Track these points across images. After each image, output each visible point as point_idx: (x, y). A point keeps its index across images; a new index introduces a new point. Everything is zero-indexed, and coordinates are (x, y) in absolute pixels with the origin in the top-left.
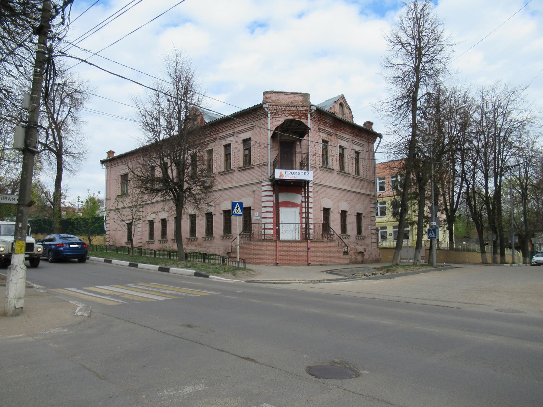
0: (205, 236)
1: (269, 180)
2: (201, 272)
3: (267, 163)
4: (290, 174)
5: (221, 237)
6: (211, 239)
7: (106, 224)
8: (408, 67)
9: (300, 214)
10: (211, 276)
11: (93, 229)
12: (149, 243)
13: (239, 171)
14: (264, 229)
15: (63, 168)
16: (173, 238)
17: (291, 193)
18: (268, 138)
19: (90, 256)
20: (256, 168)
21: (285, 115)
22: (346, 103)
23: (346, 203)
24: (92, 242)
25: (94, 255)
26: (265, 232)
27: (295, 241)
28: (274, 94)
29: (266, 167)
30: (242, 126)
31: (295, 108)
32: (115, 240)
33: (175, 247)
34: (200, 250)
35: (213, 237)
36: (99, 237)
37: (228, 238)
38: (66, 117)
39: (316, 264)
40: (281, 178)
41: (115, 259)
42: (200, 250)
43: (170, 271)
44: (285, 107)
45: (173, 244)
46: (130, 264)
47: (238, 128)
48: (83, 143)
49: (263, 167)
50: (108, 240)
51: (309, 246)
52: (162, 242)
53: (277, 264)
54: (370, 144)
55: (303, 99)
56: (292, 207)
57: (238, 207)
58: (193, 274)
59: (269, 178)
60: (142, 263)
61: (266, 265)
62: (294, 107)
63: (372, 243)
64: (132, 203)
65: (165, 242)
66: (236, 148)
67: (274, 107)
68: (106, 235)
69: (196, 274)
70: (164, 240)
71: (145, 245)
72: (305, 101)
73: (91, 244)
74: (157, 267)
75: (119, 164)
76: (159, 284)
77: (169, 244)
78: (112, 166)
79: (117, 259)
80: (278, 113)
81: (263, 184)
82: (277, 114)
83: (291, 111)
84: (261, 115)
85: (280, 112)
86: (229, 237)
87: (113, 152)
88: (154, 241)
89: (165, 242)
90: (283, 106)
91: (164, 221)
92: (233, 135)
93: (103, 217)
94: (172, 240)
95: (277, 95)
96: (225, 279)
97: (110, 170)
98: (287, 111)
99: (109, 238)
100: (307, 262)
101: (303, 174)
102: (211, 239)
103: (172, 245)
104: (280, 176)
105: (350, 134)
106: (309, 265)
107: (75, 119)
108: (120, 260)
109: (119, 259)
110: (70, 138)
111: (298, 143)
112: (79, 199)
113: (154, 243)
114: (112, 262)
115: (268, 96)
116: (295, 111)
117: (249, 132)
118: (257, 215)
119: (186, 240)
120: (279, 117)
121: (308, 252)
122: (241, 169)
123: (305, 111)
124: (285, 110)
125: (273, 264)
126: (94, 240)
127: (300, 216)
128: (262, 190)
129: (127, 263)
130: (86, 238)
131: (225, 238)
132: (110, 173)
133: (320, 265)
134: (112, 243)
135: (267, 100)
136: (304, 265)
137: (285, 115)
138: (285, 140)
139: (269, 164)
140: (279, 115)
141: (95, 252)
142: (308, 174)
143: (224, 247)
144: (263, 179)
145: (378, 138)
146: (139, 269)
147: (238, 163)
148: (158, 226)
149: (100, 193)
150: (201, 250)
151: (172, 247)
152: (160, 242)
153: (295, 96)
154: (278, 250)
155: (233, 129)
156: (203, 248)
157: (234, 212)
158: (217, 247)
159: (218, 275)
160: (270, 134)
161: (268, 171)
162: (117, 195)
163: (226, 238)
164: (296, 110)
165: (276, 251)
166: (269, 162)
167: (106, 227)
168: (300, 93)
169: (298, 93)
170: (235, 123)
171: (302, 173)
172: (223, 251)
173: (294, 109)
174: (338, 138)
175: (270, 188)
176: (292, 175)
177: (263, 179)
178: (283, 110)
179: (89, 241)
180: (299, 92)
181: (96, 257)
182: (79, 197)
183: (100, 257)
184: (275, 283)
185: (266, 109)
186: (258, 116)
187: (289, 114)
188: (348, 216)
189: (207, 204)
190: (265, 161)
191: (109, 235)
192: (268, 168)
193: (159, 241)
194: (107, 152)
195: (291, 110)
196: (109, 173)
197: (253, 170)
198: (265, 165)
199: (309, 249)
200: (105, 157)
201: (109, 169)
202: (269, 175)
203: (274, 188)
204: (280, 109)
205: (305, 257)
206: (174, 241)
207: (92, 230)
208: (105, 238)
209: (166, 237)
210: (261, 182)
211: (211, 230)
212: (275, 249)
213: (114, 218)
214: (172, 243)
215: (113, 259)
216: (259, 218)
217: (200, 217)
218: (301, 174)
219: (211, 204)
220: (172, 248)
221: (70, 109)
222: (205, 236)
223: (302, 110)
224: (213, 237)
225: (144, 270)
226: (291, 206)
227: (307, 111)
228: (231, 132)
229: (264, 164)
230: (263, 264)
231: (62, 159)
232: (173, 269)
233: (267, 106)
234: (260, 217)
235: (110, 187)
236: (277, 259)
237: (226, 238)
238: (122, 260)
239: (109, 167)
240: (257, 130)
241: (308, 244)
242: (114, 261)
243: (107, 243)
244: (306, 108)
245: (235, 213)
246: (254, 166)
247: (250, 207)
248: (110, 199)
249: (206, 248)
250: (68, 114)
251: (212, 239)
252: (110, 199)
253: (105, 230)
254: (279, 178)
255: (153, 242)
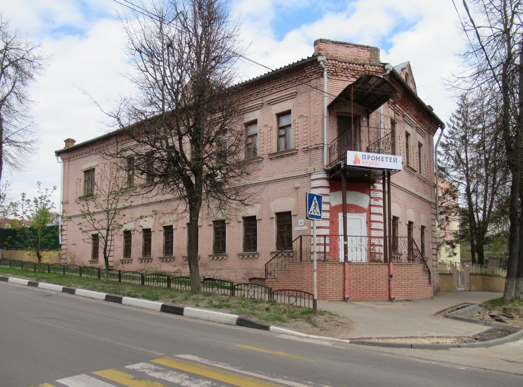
0: (212, 254)
1: (325, 170)
2: (249, 319)
3: (322, 145)
4: (370, 159)
5: (239, 255)
6: (223, 257)
7: (62, 236)
8: (495, 30)
9: (367, 223)
10: (272, 328)
11: (44, 241)
12: (124, 262)
13: (271, 159)
14: (325, 245)
15: (4, 161)
16: (162, 256)
17: (354, 192)
18: (323, 108)
19: (40, 281)
20: (300, 153)
21: (347, 77)
22: (412, 74)
23: (412, 211)
24: (42, 259)
25: (46, 280)
26: (323, 249)
27: (361, 264)
28: (330, 45)
29: (320, 151)
30: (278, 93)
31: (361, 67)
32: (75, 256)
33: (186, 271)
34: (204, 273)
35: (225, 255)
36: (51, 253)
37: (251, 257)
38: (9, 94)
39: (401, 299)
40: (357, 165)
41: (81, 288)
42: (204, 273)
43: (184, 313)
44: (347, 64)
45: (160, 264)
46: (107, 296)
47: (270, 96)
48: (31, 130)
49: (313, 152)
50: (64, 257)
51: (392, 272)
52: (143, 261)
53: (345, 300)
54: (431, 136)
55: (371, 55)
56: (356, 212)
57: (315, 203)
58: (235, 322)
59: (325, 168)
60: (129, 296)
61: (329, 301)
62: (360, 65)
63: (433, 266)
64: (108, 201)
65: (148, 261)
66: (266, 126)
67: (333, 62)
68: (62, 250)
69: (241, 322)
70: (147, 259)
71: (117, 265)
72: (374, 58)
73: (41, 262)
74: (158, 304)
75: (81, 156)
76: (206, 361)
77: (154, 265)
78: (72, 159)
79: (84, 288)
80: (336, 72)
81: (313, 177)
82: (335, 74)
83: (356, 71)
84: (311, 74)
85: (340, 71)
86: (254, 256)
87: (73, 141)
88: (132, 260)
89: (148, 261)
90: (346, 63)
91: (169, 231)
92: (257, 108)
93: (58, 226)
94: (160, 258)
95: (334, 46)
96: (306, 335)
97: (69, 164)
98: (349, 70)
99: (66, 254)
100: (388, 297)
101: (388, 160)
102: (223, 257)
103: (159, 266)
104: (355, 162)
105: (414, 118)
106: (391, 300)
107: (21, 98)
108: (89, 289)
109: (88, 288)
110: (15, 123)
111: (364, 119)
112: (23, 197)
113: (131, 263)
114: (76, 293)
115: (322, 46)
116: (360, 71)
117: (289, 101)
118: (303, 224)
119: (181, 259)
120: (338, 78)
121: (389, 280)
122: (273, 156)
123: (375, 72)
124: (347, 69)
125: (338, 299)
126: (45, 257)
127: (367, 226)
128: (312, 186)
129: (103, 295)
130: (33, 254)
131: (246, 257)
132: (69, 169)
133: (407, 300)
134: (69, 261)
135: (321, 52)
136: (383, 301)
137: (347, 77)
138: (345, 113)
139: (325, 147)
140: (337, 75)
141: (46, 275)
142: (395, 161)
143: (245, 271)
144: (315, 169)
145: (439, 128)
146: (123, 307)
147: (269, 148)
148: (138, 239)
149: (55, 189)
150: (205, 274)
151: (160, 268)
152: (140, 261)
153: (360, 50)
154: (347, 277)
155: (260, 99)
156: (209, 270)
157: (310, 212)
158: (233, 269)
159: (283, 324)
160: (327, 102)
161: (323, 157)
162: (78, 196)
163: (248, 256)
164: (363, 70)
165: (344, 279)
166: (325, 143)
167: (62, 240)
168: (367, 47)
169: (364, 47)
170: (265, 90)
171: (387, 158)
172: (243, 276)
173: (360, 68)
174: (405, 120)
175: (325, 183)
176: (372, 161)
177: (315, 169)
178: (344, 69)
179: (37, 258)
180: (366, 44)
181: (49, 283)
182: (24, 194)
183: (55, 283)
184: (411, 346)
185: (322, 63)
186: (306, 76)
187: (353, 75)
188: (414, 228)
189: (240, 201)
190: (317, 143)
191: (66, 250)
192: (323, 153)
193: (139, 259)
194: (65, 141)
195: (356, 69)
196: (67, 168)
197: (294, 157)
198: (317, 148)
199: (392, 276)
200: (62, 146)
201: (67, 163)
202: (326, 163)
203: (330, 184)
204: (341, 66)
205: (386, 289)
206: (163, 260)
207: (42, 242)
208: (59, 254)
209: (150, 254)
210: (310, 174)
211: (221, 246)
212: (341, 276)
213: (81, 223)
214: (159, 262)
215: (78, 288)
216: (306, 228)
217: (233, 223)
218: (385, 159)
219: (246, 202)
220: (159, 269)
221: (14, 83)
222: (212, 254)
223: (372, 70)
224: (225, 255)
225: (134, 309)
226: (354, 211)
227: (378, 72)
228: (258, 103)
229: (316, 146)
230: (325, 299)
231: (2, 149)
232: (189, 310)
233: (324, 58)
234: (307, 227)
235: (68, 187)
236: (346, 292)
237: (248, 256)
238: (93, 290)
239: (67, 161)
240: (302, 98)
241: (389, 268)
242: (80, 291)
243: (63, 260)
244: (377, 68)
245: (313, 214)
246: (298, 150)
247: (255, 217)
248: (68, 203)
249: (214, 271)
250: (11, 90)
251: (225, 258)
252: (68, 203)
253: (60, 243)
254: (353, 164)
255: (130, 261)
